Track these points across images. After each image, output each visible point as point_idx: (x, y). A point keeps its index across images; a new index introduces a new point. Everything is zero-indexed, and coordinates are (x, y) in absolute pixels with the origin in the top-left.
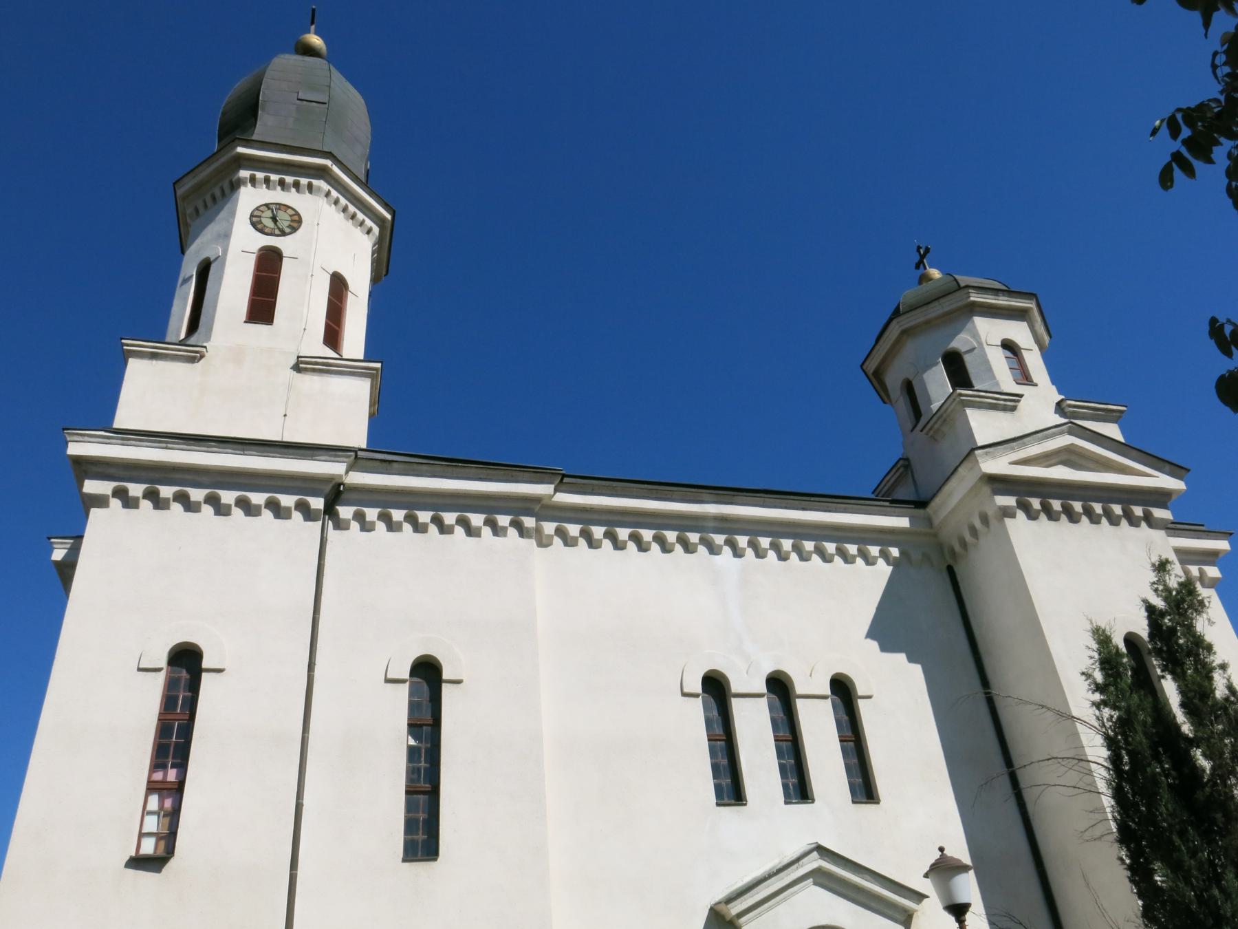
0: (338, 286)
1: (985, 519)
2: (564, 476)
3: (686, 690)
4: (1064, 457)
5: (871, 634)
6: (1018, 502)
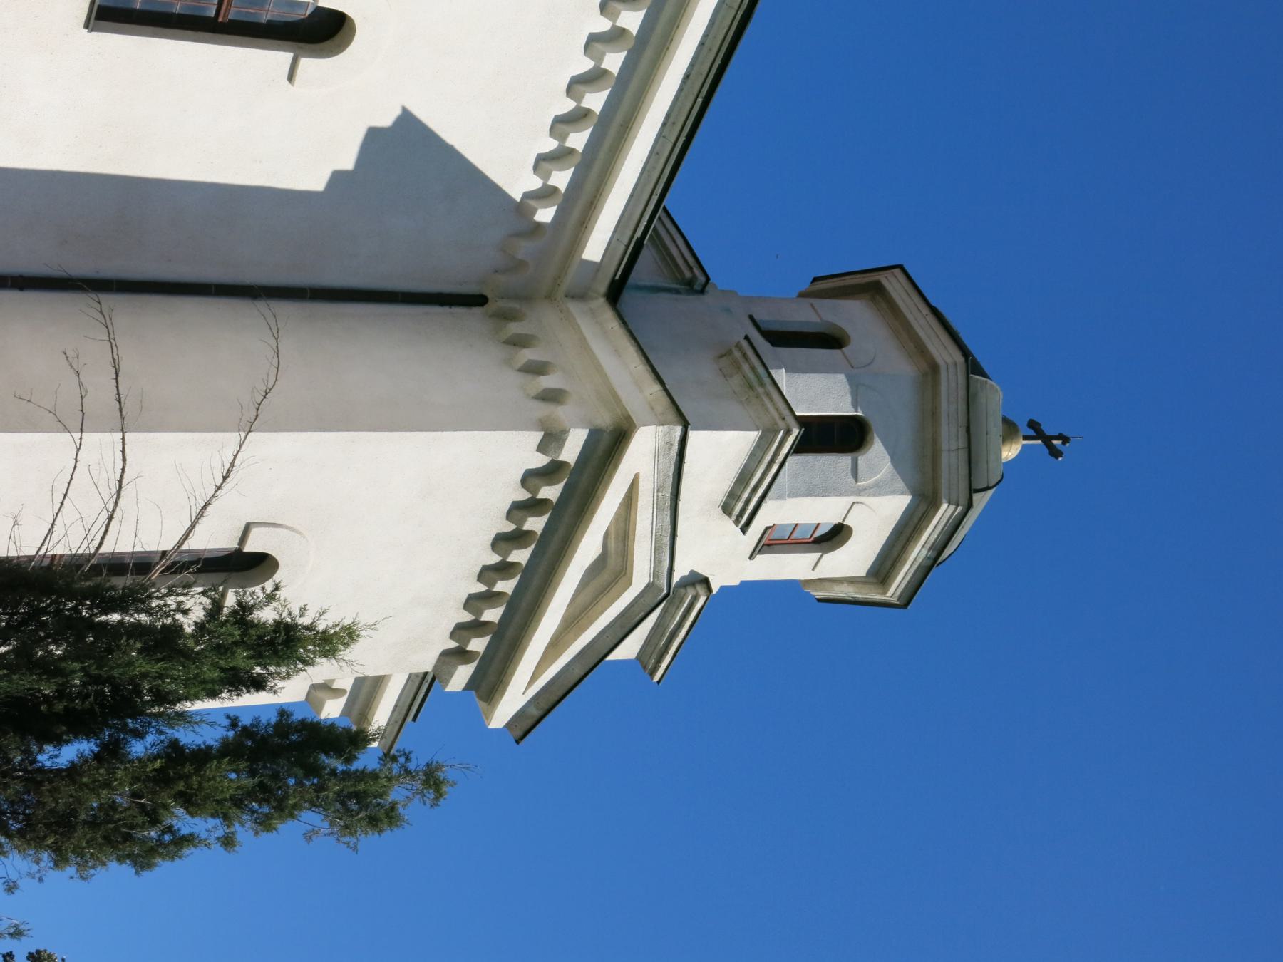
1: (552, 397)
4: (613, 561)
5: (407, 120)
6: (564, 464)
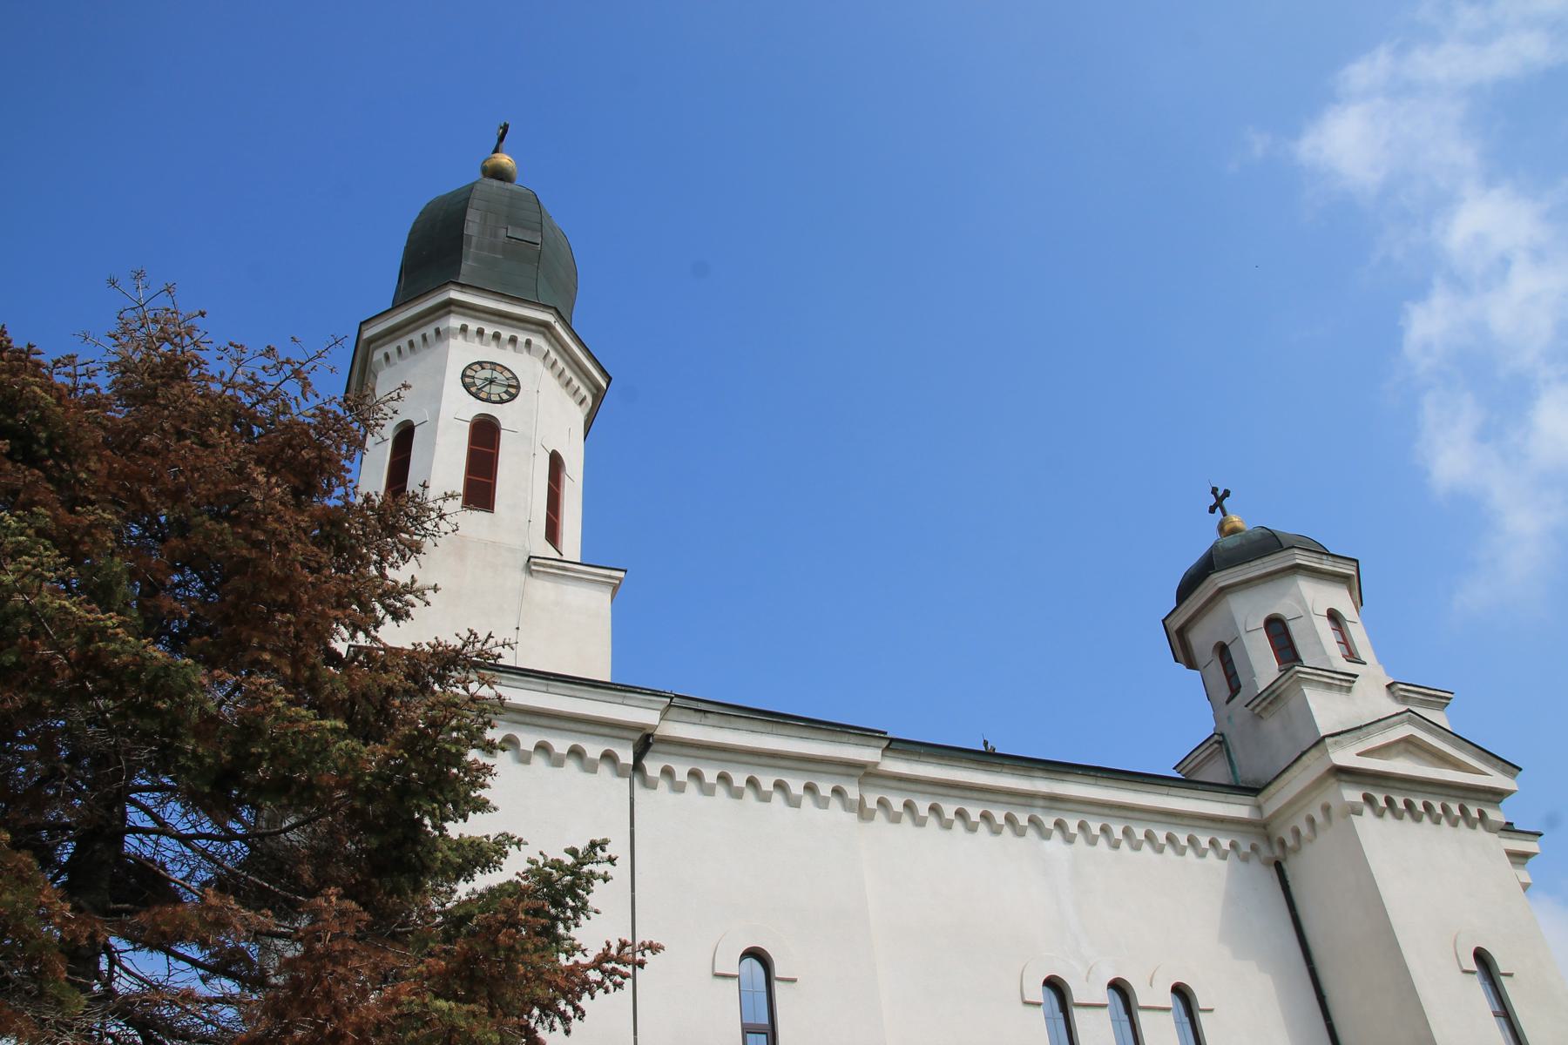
0: (556, 462)
2: (892, 740)
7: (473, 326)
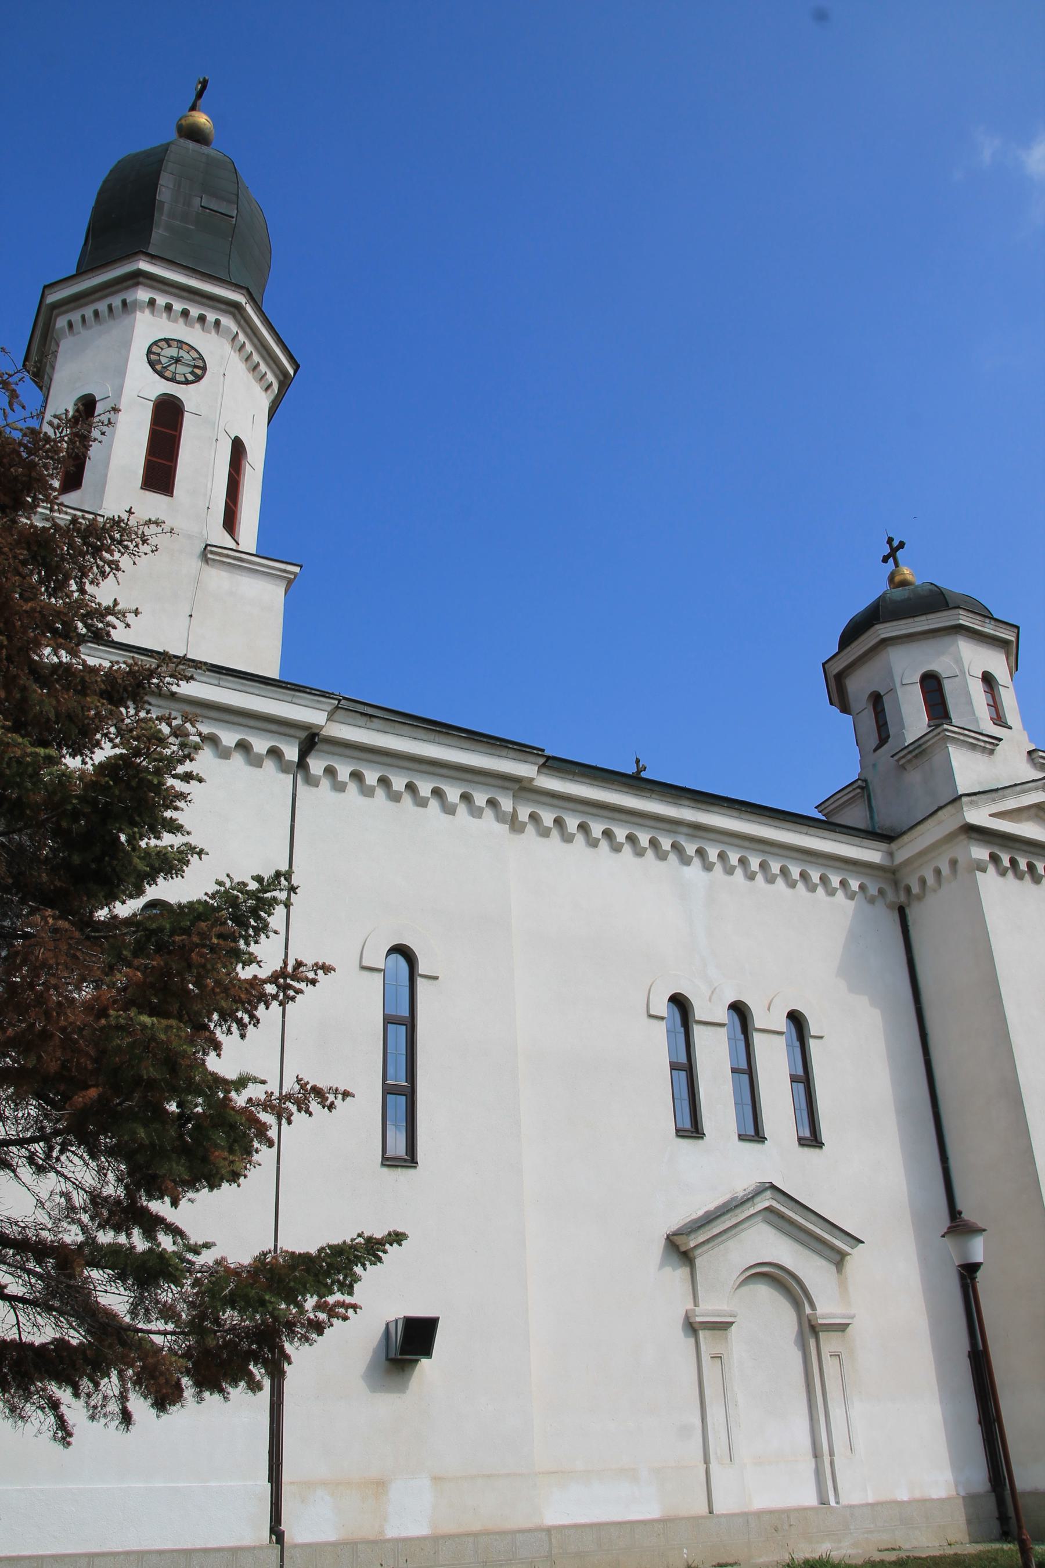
0: (238, 449)
3: (652, 1013)
7: (161, 300)
